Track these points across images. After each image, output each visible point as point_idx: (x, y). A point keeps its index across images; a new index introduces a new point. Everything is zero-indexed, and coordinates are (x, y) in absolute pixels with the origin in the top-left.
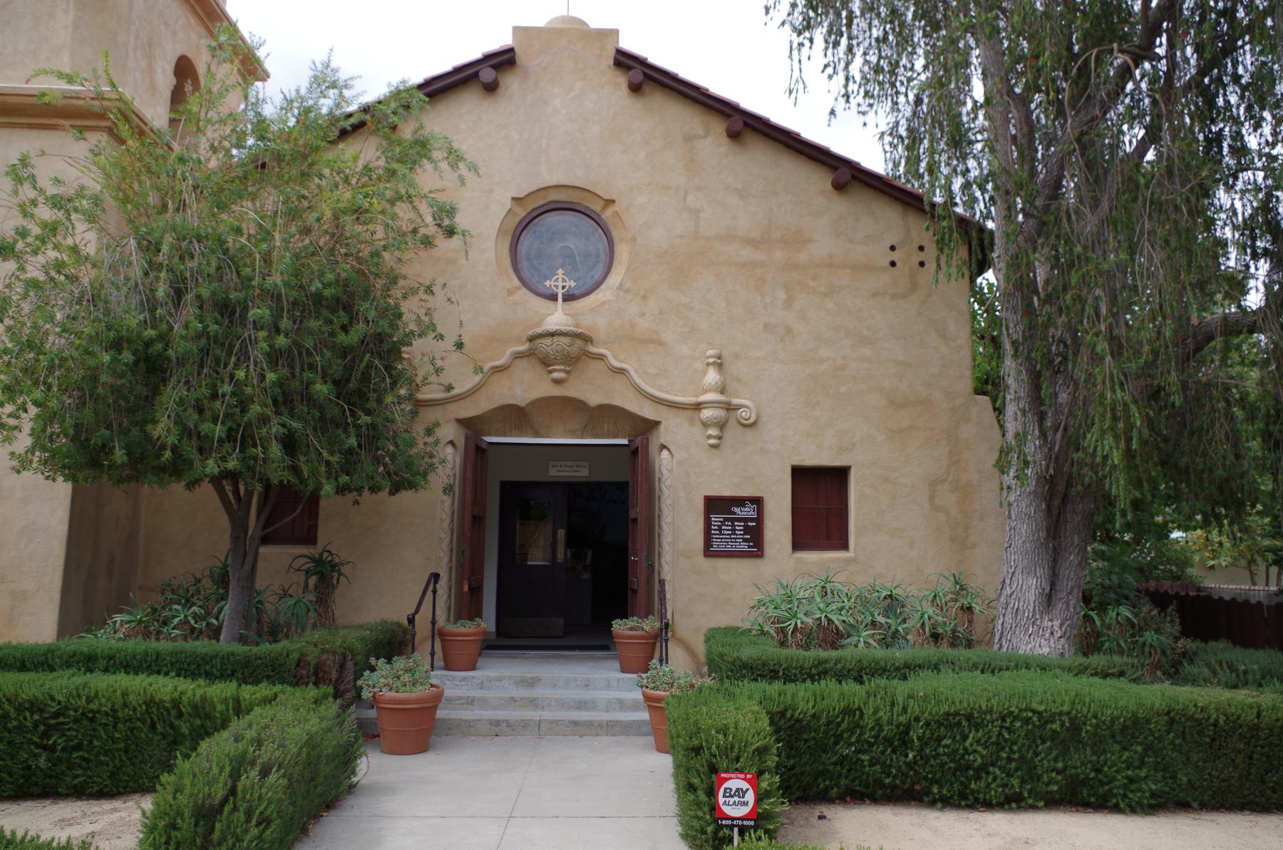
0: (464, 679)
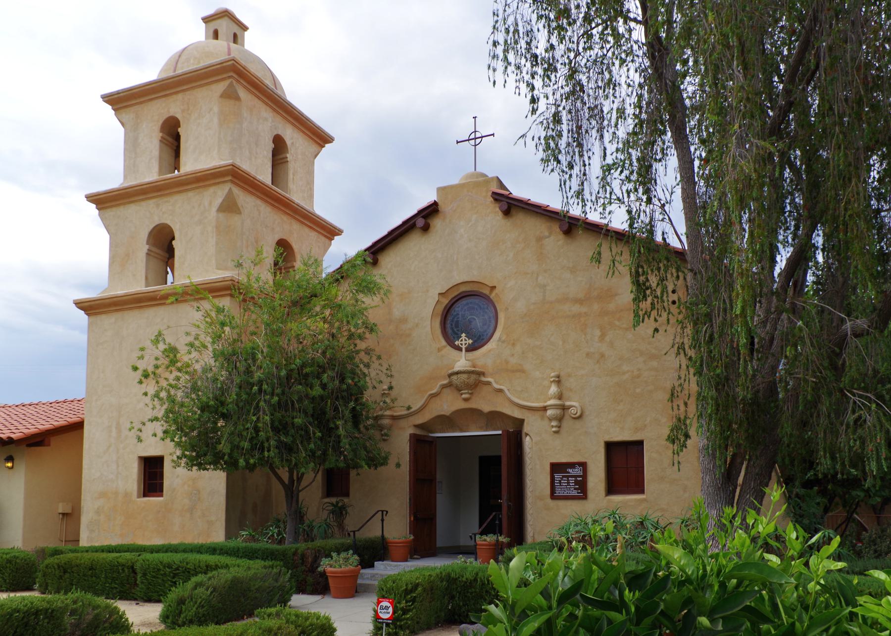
0: (395, 566)
